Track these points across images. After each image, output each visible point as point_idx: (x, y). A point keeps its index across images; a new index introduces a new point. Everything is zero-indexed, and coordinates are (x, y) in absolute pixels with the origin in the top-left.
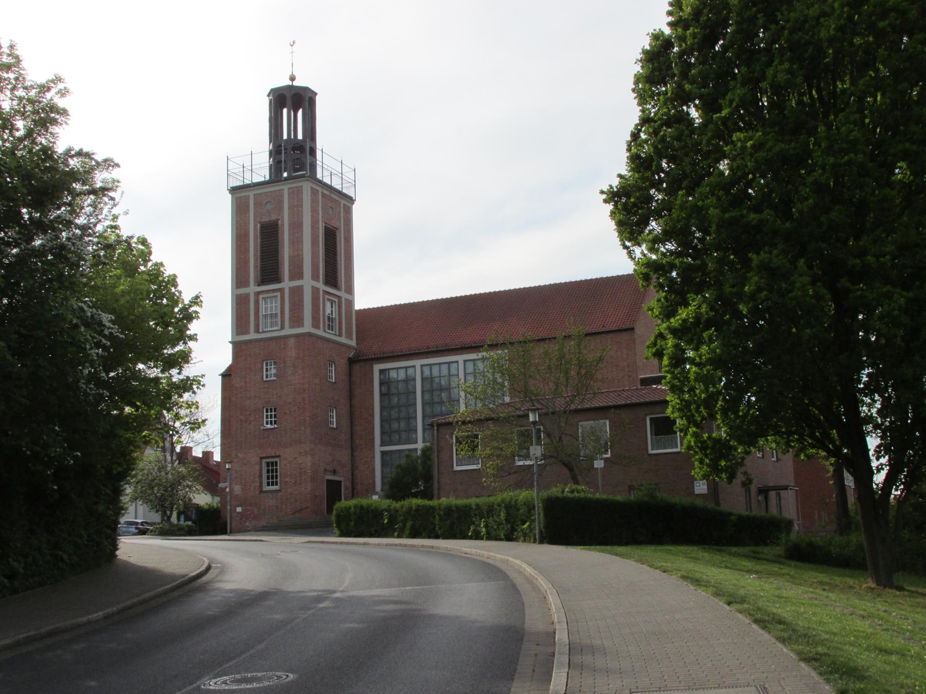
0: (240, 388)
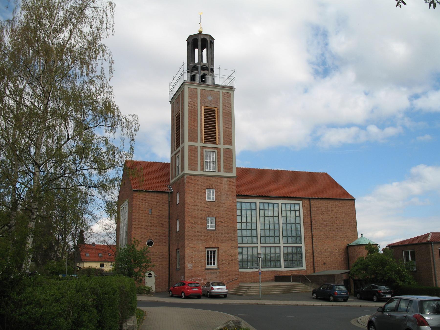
0: (191, 203)
